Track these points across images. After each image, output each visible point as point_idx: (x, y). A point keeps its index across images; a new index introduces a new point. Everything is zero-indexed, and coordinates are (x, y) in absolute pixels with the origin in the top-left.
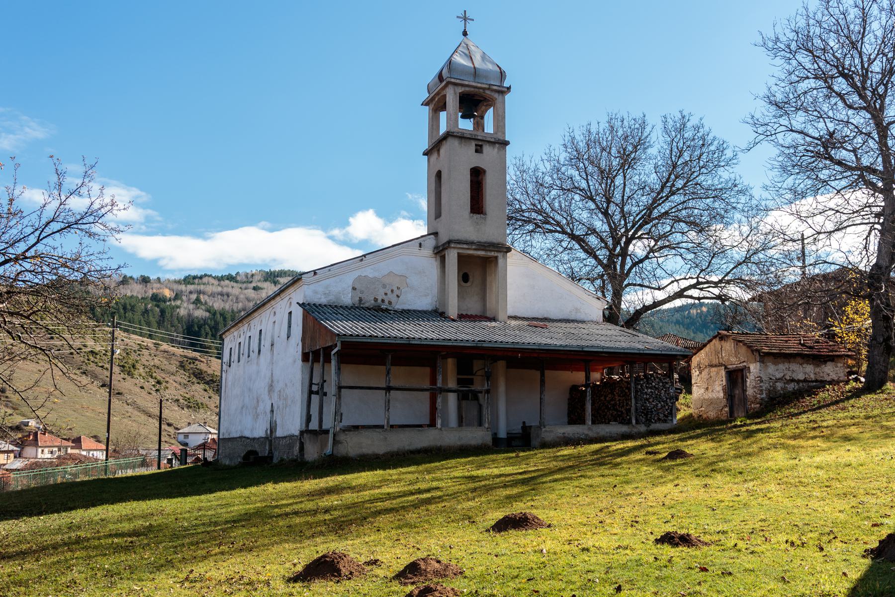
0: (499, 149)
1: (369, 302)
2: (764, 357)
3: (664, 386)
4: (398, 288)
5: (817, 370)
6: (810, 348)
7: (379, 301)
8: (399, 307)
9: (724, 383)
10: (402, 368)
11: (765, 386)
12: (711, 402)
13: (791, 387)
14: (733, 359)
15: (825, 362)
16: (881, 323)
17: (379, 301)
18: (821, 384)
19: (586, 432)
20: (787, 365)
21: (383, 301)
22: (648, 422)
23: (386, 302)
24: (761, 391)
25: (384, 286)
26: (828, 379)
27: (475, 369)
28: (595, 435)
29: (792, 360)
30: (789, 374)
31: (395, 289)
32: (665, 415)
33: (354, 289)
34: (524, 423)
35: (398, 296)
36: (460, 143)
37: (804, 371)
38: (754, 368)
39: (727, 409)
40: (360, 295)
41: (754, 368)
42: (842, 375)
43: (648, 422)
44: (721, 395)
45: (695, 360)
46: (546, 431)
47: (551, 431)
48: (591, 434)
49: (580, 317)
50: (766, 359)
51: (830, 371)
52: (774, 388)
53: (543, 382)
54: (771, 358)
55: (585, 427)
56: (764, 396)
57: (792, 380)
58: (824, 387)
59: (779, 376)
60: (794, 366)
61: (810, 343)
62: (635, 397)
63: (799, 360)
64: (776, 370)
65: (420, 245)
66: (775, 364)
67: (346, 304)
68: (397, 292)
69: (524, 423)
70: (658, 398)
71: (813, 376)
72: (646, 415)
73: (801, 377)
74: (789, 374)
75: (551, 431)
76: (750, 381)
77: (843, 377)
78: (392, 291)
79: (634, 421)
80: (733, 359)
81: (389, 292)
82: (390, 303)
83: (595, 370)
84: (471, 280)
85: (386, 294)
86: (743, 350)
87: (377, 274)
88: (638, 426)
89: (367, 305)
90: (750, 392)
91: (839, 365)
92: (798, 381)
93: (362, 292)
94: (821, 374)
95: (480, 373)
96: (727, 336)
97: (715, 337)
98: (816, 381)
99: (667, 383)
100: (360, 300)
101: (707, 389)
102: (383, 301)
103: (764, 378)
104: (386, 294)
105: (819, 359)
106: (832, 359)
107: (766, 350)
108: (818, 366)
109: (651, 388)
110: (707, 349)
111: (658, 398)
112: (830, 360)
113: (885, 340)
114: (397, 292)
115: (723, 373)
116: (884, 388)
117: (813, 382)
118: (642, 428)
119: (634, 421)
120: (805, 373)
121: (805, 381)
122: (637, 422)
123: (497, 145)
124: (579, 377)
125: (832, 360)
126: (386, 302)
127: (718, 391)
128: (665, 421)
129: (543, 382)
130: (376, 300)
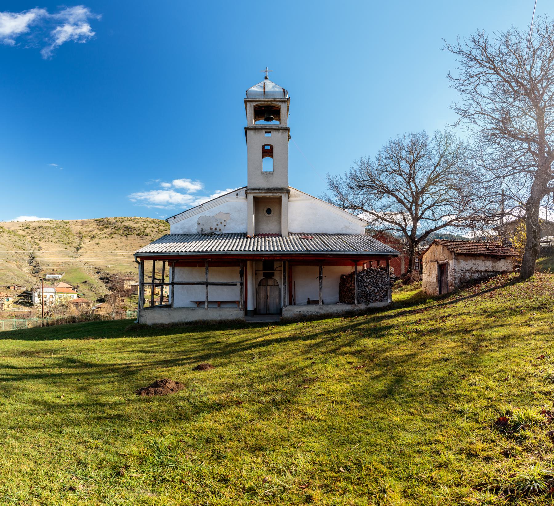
0: (282, 133)
1: (207, 231)
2: (458, 256)
3: (381, 277)
4: (225, 221)
5: (494, 264)
6: (491, 250)
7: (214, 229)
8: (224, 232)
9: (437, 272)
10: (228, 268)
11: (458, 275)
12: (431, 284)
13: (476, 275)
14: (442, 257)
15: (500, 260)
16: (532, 235)
17: (214, 229)
18: (495, 274)
19: (318, 310)
20: (473, 261)
21: (216, 229)
22: (368, 302)
23: (218, 230)
24: (455, 278)
25: (216, 221)
26: (501, 270)
27: (275, 266)
28: (325, 312)
29: (478, 258)
30: (475, 267)
31: (223, 221)
32: (381, 297)
33: (199, 224)
34: (308, 299)
35: (225, 226)
36: (255, 133)
37: (488, 265)
38: (452, 263)
39: (438, 289)
40: (202, 227)
41: (452, 263)
42: (510, 268)
43: (368, 302)
44: (435, 280)
45: (424, 257)
46: (286, 310)
47: (289, 310)
48: (322, 312)
49: (347, 232)
50: (459, 257)
51: (502, 265)
52: (464, 276)
53: (321, 273)
54: (463, 257)
55: (318, 307)
56: (457, 281)
57: (477, 271)
58: (497, 276)
59: (468, 268)
60: (479, 262)
61: (493, 247)
62: (358, 285)
63: (483, 258)
64: (465, 265)
65: (237, 195)
66: (466, 260)
67: (194, 233)
68: (223, 224)
69: (308, 299)
70: (376, 285)
71: (491, 269)
72: (366, 297)
73: (483, 269)
74: (475, 267)
75: (289, 310)
76: (450, 272)
77: (511, 269)
78: (221, 223)
79: (356, 302)
80: (442, 257)
81: (219, 224)
82: (220, 230)
83: (360, 265)
84: (272, 212)
85: (217, 225)
86: (446, 251)
87: (212, 214)
88: (359, 305)
89: (206, 232)
90: (449, 279)
91: (509, 261)
92: (481, 272)
93: (203, 225)
94: (497, 267)
95: (278, 269)
96: (439, 242)
97: (433, 243)
98: (493, 271)
99: (383, 274)
100: (202, 230)
101: (429, 275)
102: (216, 229)
103: (457, 270)
104: (217, 225)
105: (496, 258)
106: (504, 257)
107: (459, 251)
108: (495, 262)
109: (370, 278)
110: (429, 250)
111: (376, 285)
112: (503, 258)
113: (533, 247)
114: (223, 224)
115: (436, 266)
116: (531, 278)
117: (491, 272)
118: (363, 307)
119: (356, 302)
120: (486, 267)
121: (486, 271)
122: (359, 303)
123: (281, 131)
124: (348, 269)
125: (504, 259)
126: (218, 230)
127: (433, 278)
128: (381, 301)
129: (321, 273)
130: (211, 229)
